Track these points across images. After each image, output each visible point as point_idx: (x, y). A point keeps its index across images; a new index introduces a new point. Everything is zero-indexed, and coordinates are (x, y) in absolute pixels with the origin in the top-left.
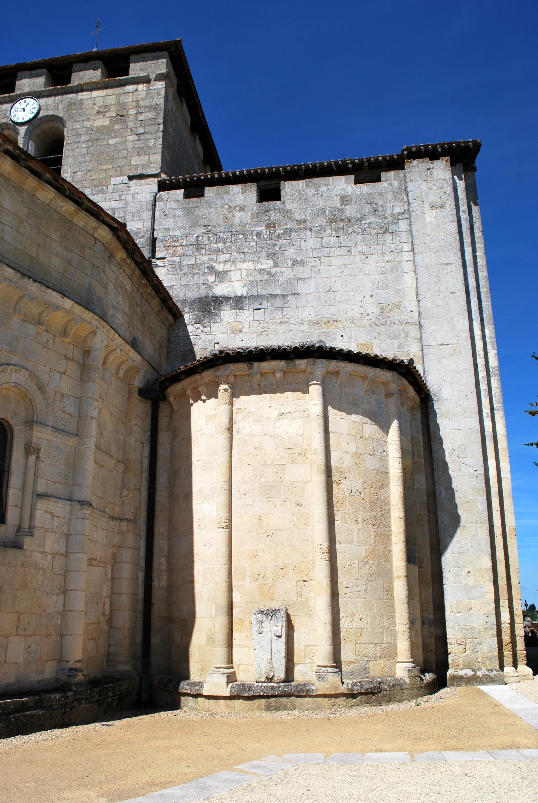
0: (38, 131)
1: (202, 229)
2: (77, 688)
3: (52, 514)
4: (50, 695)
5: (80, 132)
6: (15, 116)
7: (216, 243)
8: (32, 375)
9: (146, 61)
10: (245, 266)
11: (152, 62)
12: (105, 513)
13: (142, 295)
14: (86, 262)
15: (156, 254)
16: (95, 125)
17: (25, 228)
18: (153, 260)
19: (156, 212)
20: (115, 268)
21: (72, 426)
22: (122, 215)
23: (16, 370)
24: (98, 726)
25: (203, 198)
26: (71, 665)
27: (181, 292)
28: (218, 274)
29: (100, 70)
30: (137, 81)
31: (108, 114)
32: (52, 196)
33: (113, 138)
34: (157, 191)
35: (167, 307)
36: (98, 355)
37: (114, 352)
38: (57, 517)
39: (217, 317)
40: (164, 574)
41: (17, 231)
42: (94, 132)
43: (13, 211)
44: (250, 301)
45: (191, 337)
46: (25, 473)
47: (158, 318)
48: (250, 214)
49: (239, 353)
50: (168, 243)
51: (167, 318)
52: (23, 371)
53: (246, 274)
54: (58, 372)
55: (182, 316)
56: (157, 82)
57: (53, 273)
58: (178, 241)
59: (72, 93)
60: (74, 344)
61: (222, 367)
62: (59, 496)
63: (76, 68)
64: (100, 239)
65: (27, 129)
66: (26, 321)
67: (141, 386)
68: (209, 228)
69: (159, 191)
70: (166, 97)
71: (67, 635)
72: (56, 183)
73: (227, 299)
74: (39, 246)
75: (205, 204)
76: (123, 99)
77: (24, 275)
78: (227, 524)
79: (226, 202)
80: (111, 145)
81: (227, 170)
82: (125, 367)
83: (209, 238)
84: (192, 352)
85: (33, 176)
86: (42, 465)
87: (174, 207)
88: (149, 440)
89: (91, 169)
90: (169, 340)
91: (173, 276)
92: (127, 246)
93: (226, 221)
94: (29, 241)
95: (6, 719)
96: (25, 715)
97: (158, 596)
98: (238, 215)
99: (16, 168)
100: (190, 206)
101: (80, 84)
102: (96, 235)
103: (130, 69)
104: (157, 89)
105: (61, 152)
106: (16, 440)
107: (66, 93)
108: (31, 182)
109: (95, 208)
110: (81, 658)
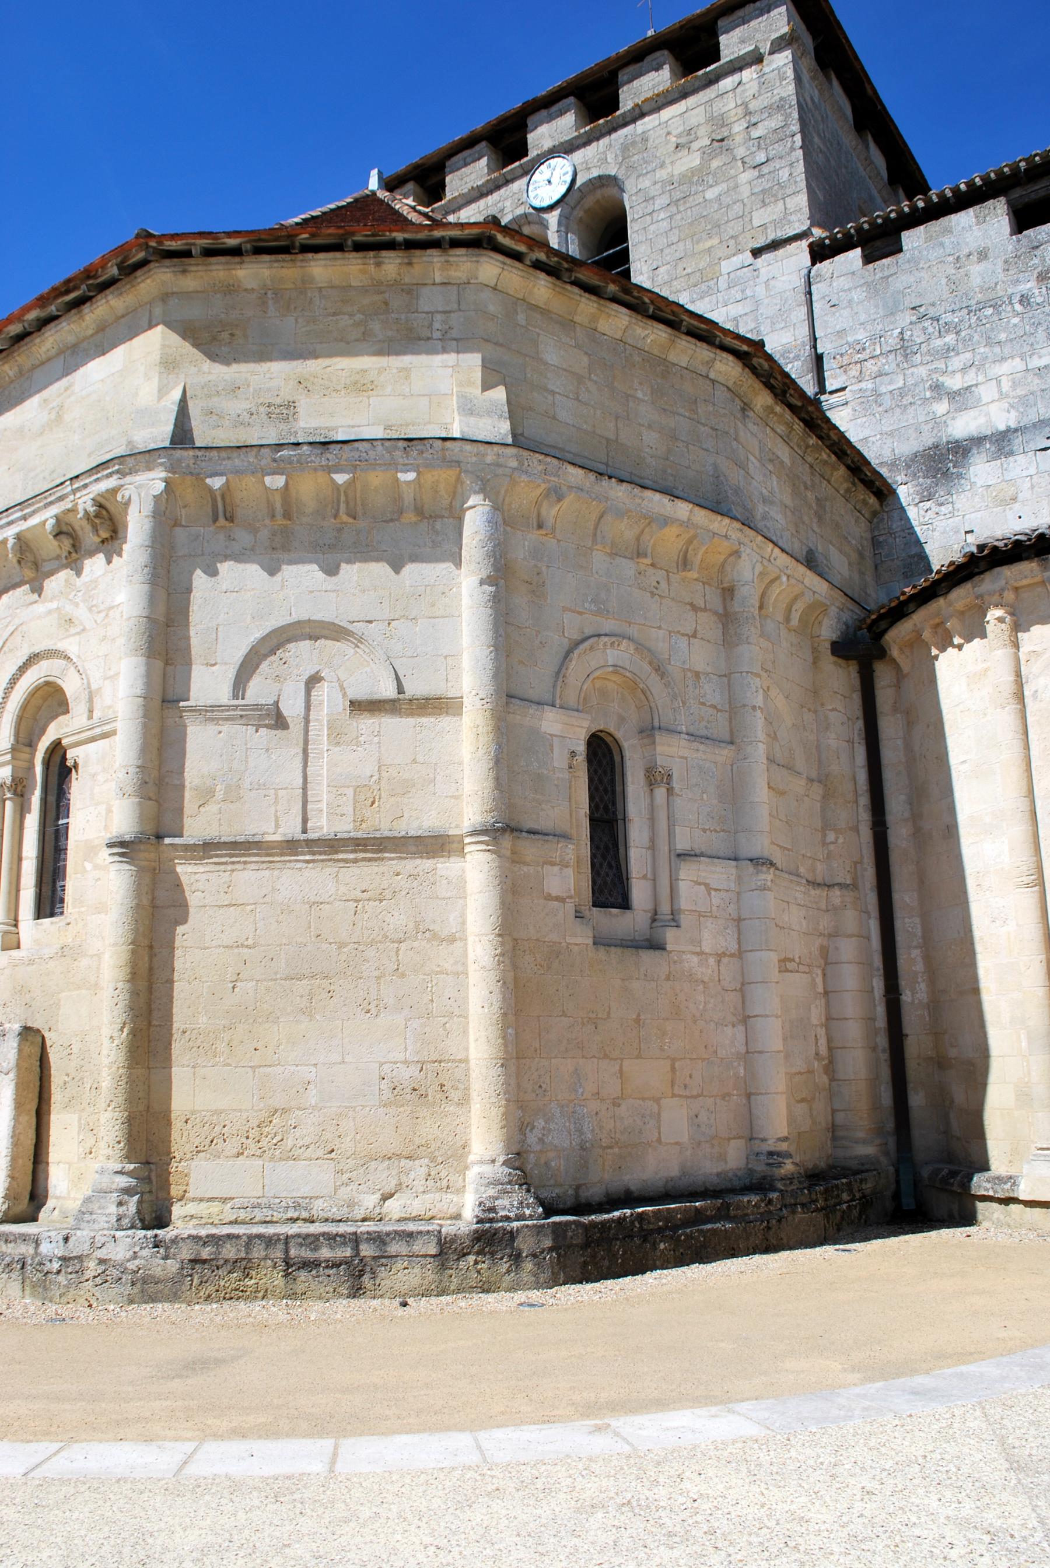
0: (579, 213)
1: (907, 317)
2: (785, 1185)
3: (706, 885)
4: (740, 1197)
5: (652, 193)
6: (536, 197)
7: (940, 337)
8: (640, 647)
9: (749, 22)
10: (1005, 368)
11: (760, 19)
12: (798, 876)
13: (811, 467)
14: (703, 429)
15: (827, 383)
16: (676, 172)
17: (589, 392)
18: (823, 398)
19: (815, 305)
20: (755, 427)
21: (721, 729)
22: (753, 326)
23: (612, 644)
24: (828, 1250)
25: (901, 255)
26: (771, 1145)
27: (886, 447)
28: (953, 396)
29: (667, 67)
30: (737, 65)
31: (695, 146)
32: (626, 323)
33: (711, 186)
34: (809, 264)
35: (862, 481)
36: (749, 594)
37: (777, 583)
38: (716, 890)
39: (963, 481)
40: (920, 980)
41: (577, 399)
42: (675, 185)
43: (564, 367)
44: (1027, 436)
45: (916, 529)
46: (652, 820)
47: (849, 506)
48: (1000, 263)
49: (1017, 543)
50: (846, 357)
51: (865, 502)
52: (625, 642)
53: (1010, 384)
54: (683, 635)
55: (894, 492)
56: (776, 56)
57: (649, 460)
58: (864, 349)
59: (625, 125)
60: (704, 580)
61: (987, 576)
62: (714, 854)
63: (625, 78)
64: (721, 379)
65: (560, 215)
66: (616, 554)
67: (834, 637)
68: (922, 310)
69: (813, 264)
70: (798, 79)
71: (758, 1094)
72: (627, 297)
73: (978, 441)
74: (617, 418)
75: (907, 266)
76: (719, 107)
77: (601, 474)
78: (1033, 877)
79: (948, 251)
80: (711, 201)
81: (940, 186)
82: (799, 606)
83: (924, 329)
84: (922, 558)
85: (587, 295)
86: (678, 802)
87: (846, 287)
88: (863, 736)
89: (683, 255)
90: (875, 543)
91: (864, 419)
92: (772, 381)
93: (954, 287)
94: (599, 412)
95: (672, 1238)
96: (702, 1230)
97: (913, 1021)
98: (977, 271)
99: (557, 289)
100: (877, 277)
101: (637, 105)
102: (712, 375)
103: (722, 47)
104: (778, 69)
105: (625, 239)
106: (628, 764)
107: (615, 129)
108: (586, 306)
109: (703, 326)
110: (786, 1134)
